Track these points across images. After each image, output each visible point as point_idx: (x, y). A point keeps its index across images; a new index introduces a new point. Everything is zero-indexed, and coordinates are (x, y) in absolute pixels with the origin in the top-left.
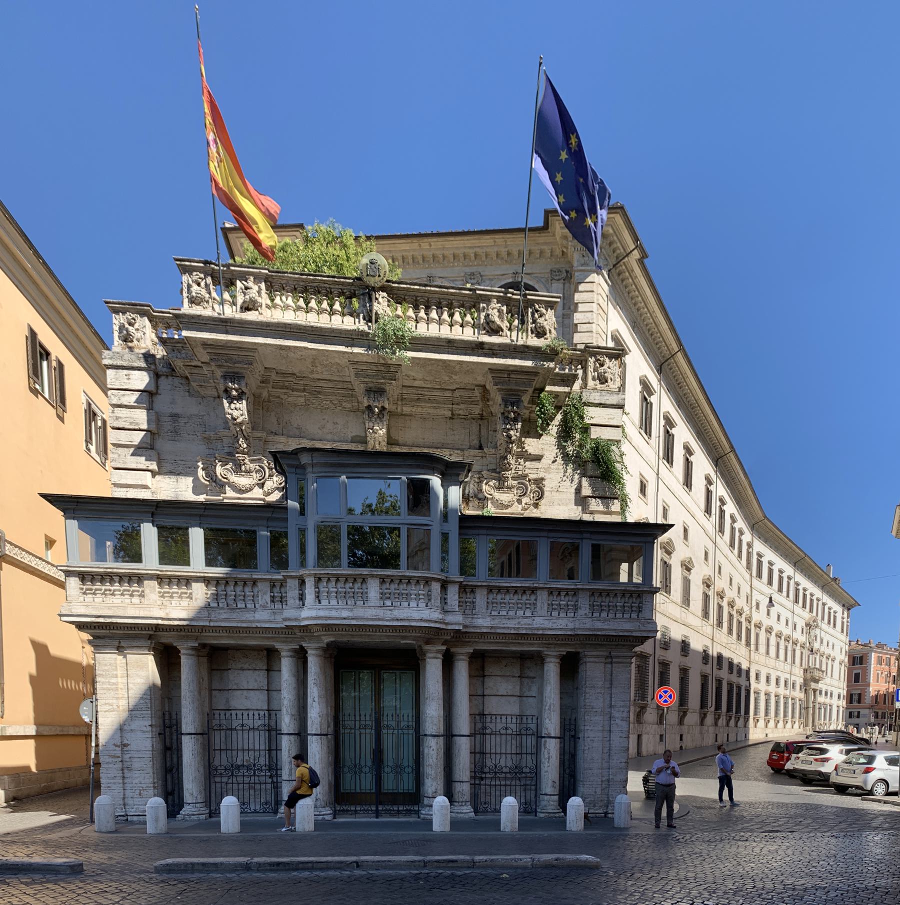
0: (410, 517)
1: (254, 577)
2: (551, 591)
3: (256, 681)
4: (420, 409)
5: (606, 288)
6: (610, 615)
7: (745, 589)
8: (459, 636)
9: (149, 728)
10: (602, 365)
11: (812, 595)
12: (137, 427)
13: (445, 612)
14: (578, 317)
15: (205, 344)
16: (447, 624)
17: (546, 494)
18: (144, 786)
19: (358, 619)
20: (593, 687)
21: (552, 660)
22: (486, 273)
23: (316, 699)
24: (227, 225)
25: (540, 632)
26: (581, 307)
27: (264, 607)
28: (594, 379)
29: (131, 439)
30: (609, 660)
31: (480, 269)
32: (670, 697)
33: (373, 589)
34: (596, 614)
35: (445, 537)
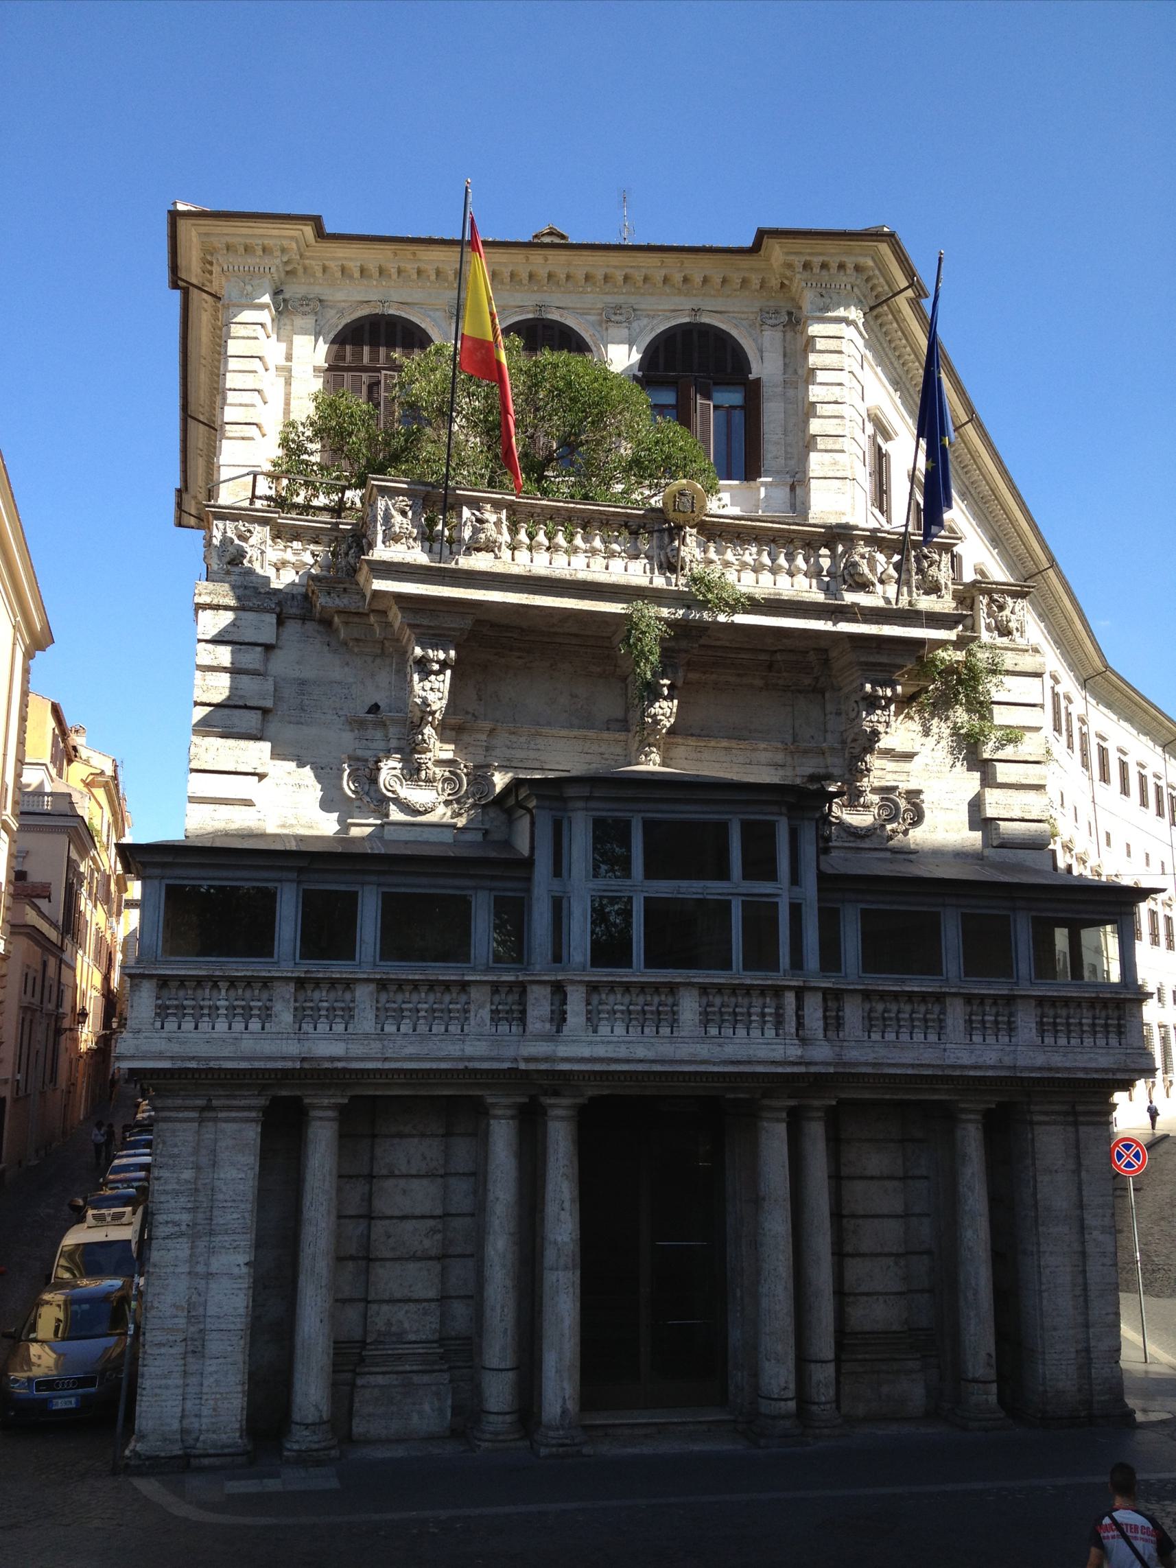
0: (748, 883)
1: (466, 978)
2: (969, 999)
4: (714, 677)
5: (860, 343)
6: (1073, 1041)
7: (1085, 813)
8: (817, 1082)
9: (244, 1270)
10: (1001, 608)
12: (241, 703)
13: (804, 1041)
14: (815, 393)
15: (400, 597)
16: (808, 1064)
17: (927, 813)
19: (662, 1062)
21: (972, 1117)
22: (643, 307)
23: (567, 1205)
24: (181, 207)
25: (958, 1073)
26: (821, 376)
27: (480, 1036)
28: (988, 628)
30: (1071, 1119)
31: (632, 300)
32: (1137, 1156)
33: (689, 1007)
34: (1049, 1040)
35: (796, 910)
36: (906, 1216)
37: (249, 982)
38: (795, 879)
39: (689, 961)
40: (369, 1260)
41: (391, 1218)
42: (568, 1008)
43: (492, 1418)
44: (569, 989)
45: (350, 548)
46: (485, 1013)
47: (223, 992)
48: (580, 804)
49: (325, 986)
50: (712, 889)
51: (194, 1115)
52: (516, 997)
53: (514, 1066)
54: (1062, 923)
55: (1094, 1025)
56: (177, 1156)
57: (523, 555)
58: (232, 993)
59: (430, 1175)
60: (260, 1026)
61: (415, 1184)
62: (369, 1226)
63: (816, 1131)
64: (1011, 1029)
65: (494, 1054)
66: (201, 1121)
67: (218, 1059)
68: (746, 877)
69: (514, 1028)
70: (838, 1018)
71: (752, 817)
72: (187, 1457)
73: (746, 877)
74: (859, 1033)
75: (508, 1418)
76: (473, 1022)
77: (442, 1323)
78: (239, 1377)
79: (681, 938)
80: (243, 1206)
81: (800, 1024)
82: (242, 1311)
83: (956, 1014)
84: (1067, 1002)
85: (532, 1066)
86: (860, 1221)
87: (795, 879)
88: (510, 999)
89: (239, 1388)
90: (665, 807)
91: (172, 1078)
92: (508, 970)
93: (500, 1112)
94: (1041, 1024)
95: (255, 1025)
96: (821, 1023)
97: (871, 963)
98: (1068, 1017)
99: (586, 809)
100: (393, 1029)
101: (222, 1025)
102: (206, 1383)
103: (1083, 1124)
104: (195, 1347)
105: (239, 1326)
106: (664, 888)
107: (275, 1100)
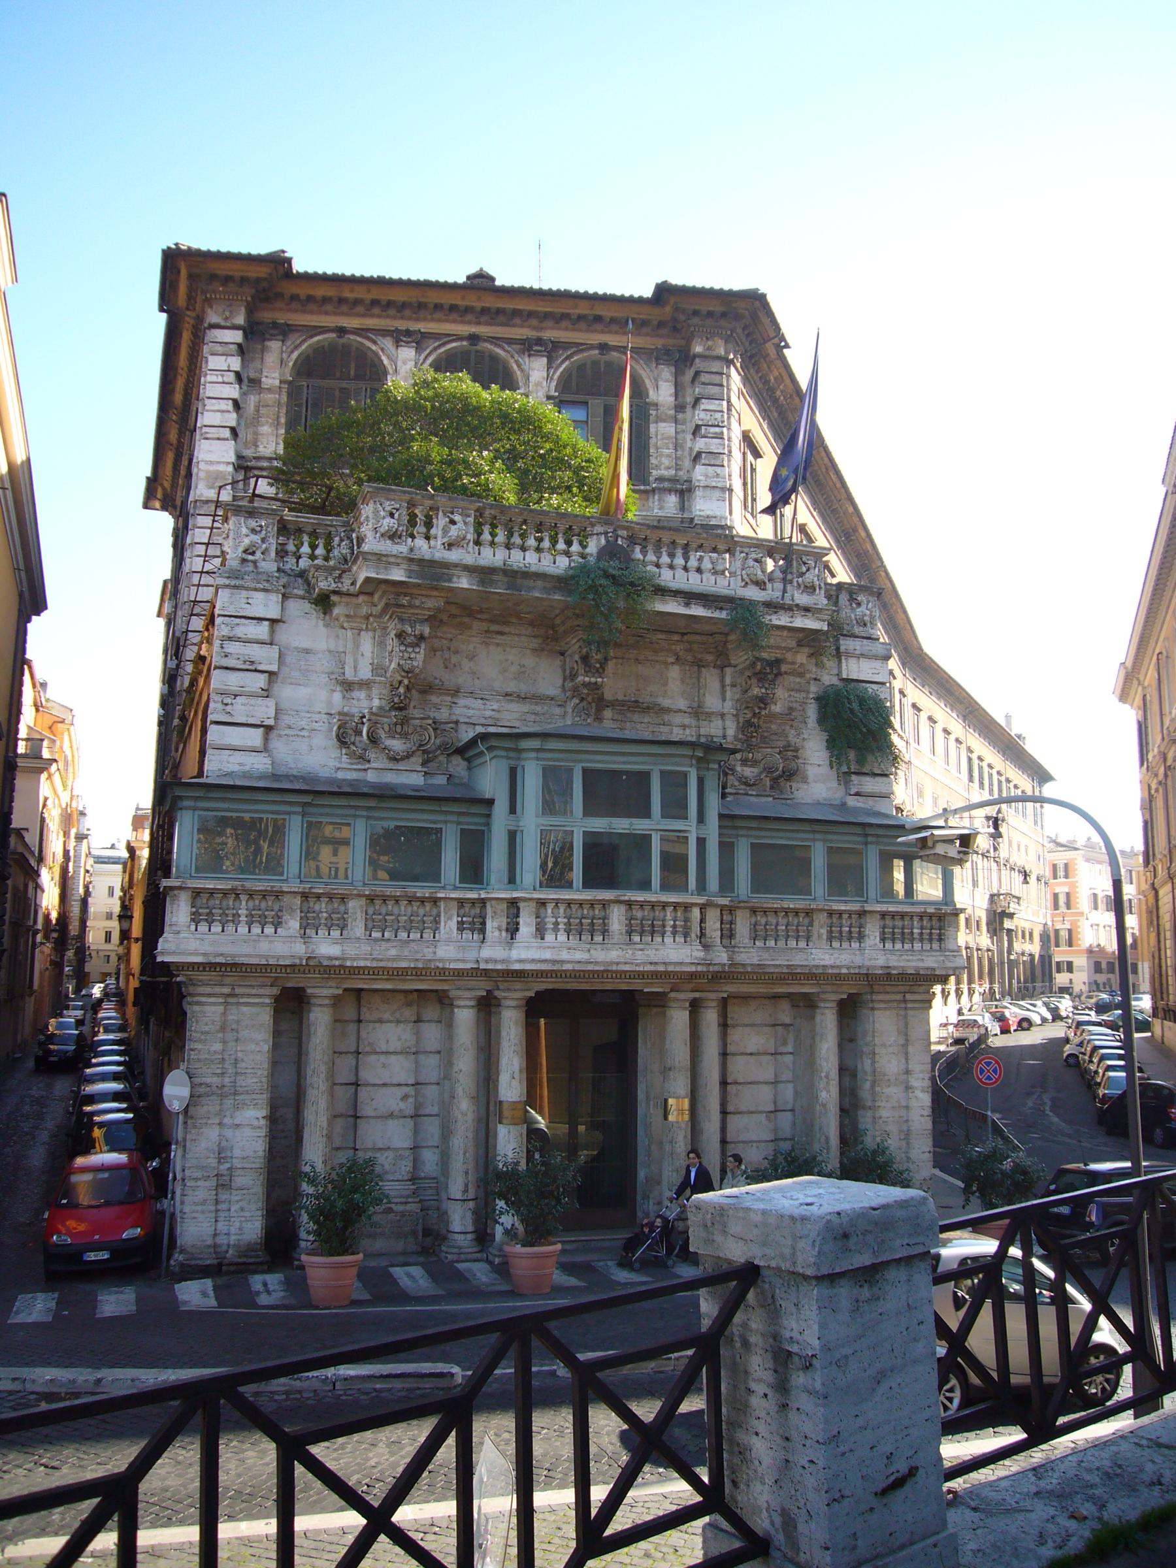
3: (400, 1039)
11: (990, 766)
13: (706, 947)
18: (247, 1214)
20: (884, 1045)
23: (517, 1075)
27: (449, 941)
29: (242, 684)
30: (903, 1005)
36: (775, 1083)
37: (264, 895)
38: (701, 819)
39: (610, 883)
40: (356, 1117)
41: (374, 1085)
42: (521, 920)
43: (456, 1236)
44: (521, 905)
45: (342, 540)
46: (453, 924)
47: (244, 903)
48: (533, 755)
49: (325, 900)
50: (640, 825)
51: (221, 1000)
52: (478, 911)
53: (475, 966)
54: (899, 857)
55: (921, 933)
56: (208, 1033)
57: (487, 552)
58: (251, 904)
59: (403, 1052)
60: (273, 930)
61: (393, 1059)
62: (356, 1091)
63: (710, 1017)
64: (861, 937)
65: (460, 956)
66: (226, 1004)
67: (241, 956)
68: (665, 815)
69: (476, 936)
70: (731, 930)
71: (669, 768)
72: (220, 1265)
73: (665, 815)
74: (746, 941)
75: (470, 1237)
76: (442, 931)
77: (415, 1168)
78: (260, 1204)
79: (608, 864)
80: (260, 1072)
81: (702, 934)
82: (261, 1154)
83: (820, 926)
84: (902, 916)
85: (490, 966)
86: (739, 1087)
87: (701, 819)
88: (473, 912)
89: (260, 1213)
90: (607, 758)
91: (204, 970)
92: (471, 890)
93: (462, 1003)
94: (883, 933)
95: (269, 930)
96: (719, 933)
97: (758, 885)
98: (903, 928)
99: (538, 759)
100: (379, 935)
101: (242, 929)
102: (233, 1209)
103: (911, 1009)
104: (223, 1183)
105: (258, 1166)
106: (599, 824)
107: (285, 990)
